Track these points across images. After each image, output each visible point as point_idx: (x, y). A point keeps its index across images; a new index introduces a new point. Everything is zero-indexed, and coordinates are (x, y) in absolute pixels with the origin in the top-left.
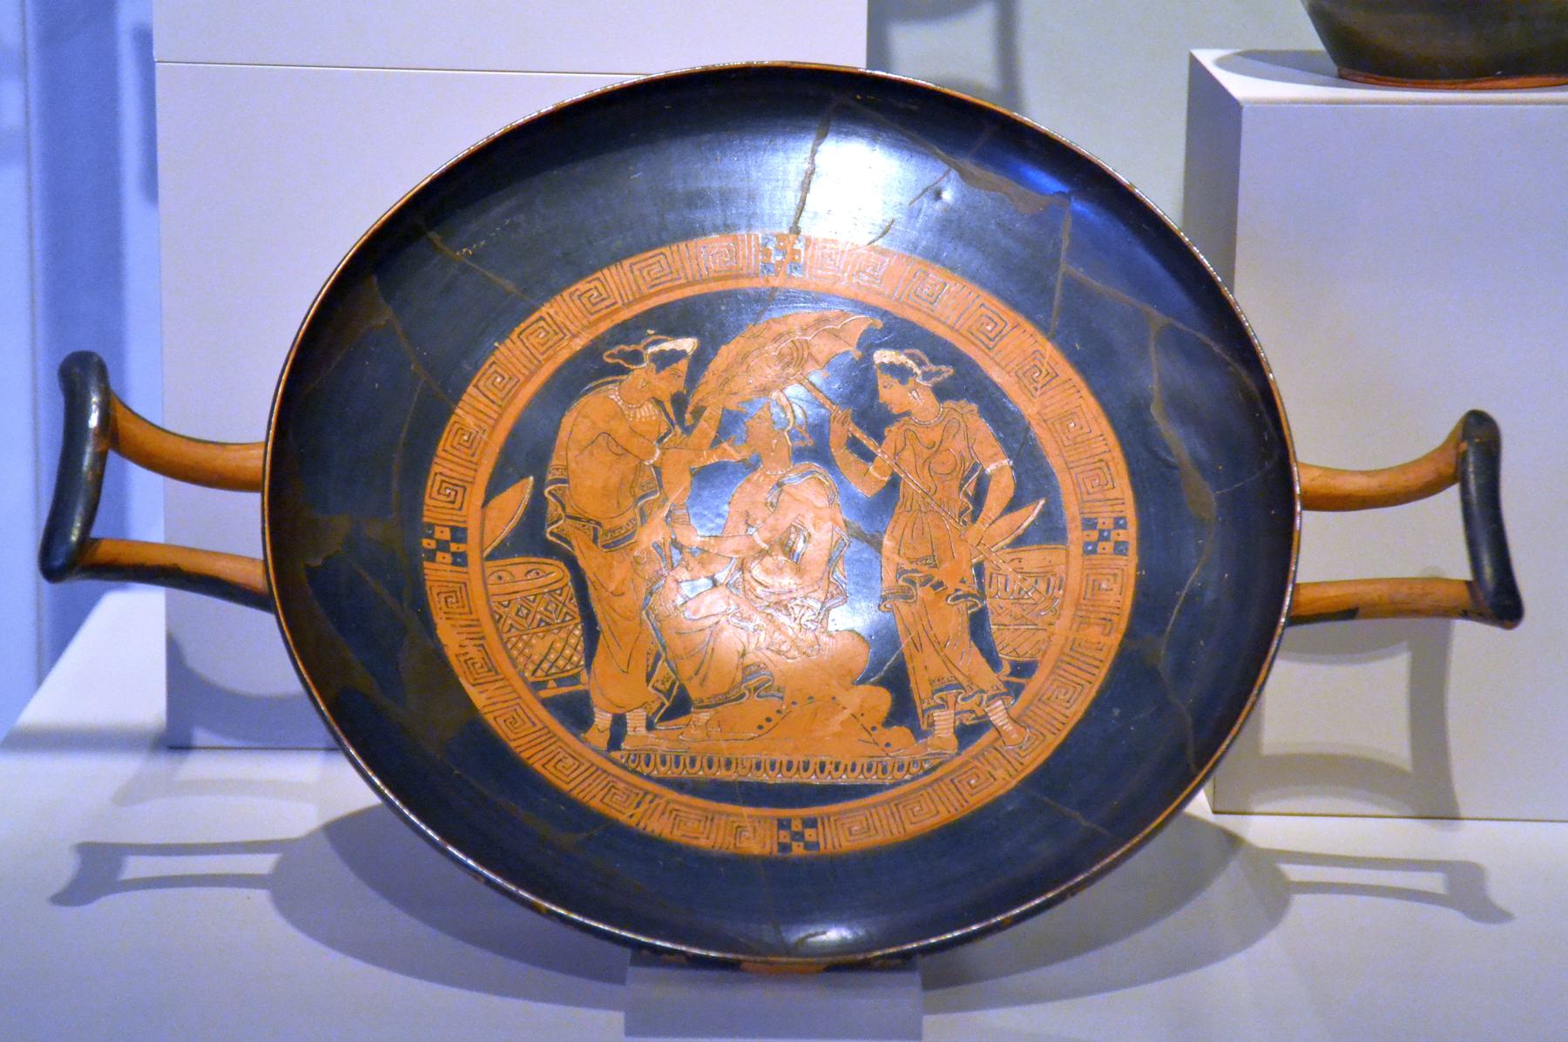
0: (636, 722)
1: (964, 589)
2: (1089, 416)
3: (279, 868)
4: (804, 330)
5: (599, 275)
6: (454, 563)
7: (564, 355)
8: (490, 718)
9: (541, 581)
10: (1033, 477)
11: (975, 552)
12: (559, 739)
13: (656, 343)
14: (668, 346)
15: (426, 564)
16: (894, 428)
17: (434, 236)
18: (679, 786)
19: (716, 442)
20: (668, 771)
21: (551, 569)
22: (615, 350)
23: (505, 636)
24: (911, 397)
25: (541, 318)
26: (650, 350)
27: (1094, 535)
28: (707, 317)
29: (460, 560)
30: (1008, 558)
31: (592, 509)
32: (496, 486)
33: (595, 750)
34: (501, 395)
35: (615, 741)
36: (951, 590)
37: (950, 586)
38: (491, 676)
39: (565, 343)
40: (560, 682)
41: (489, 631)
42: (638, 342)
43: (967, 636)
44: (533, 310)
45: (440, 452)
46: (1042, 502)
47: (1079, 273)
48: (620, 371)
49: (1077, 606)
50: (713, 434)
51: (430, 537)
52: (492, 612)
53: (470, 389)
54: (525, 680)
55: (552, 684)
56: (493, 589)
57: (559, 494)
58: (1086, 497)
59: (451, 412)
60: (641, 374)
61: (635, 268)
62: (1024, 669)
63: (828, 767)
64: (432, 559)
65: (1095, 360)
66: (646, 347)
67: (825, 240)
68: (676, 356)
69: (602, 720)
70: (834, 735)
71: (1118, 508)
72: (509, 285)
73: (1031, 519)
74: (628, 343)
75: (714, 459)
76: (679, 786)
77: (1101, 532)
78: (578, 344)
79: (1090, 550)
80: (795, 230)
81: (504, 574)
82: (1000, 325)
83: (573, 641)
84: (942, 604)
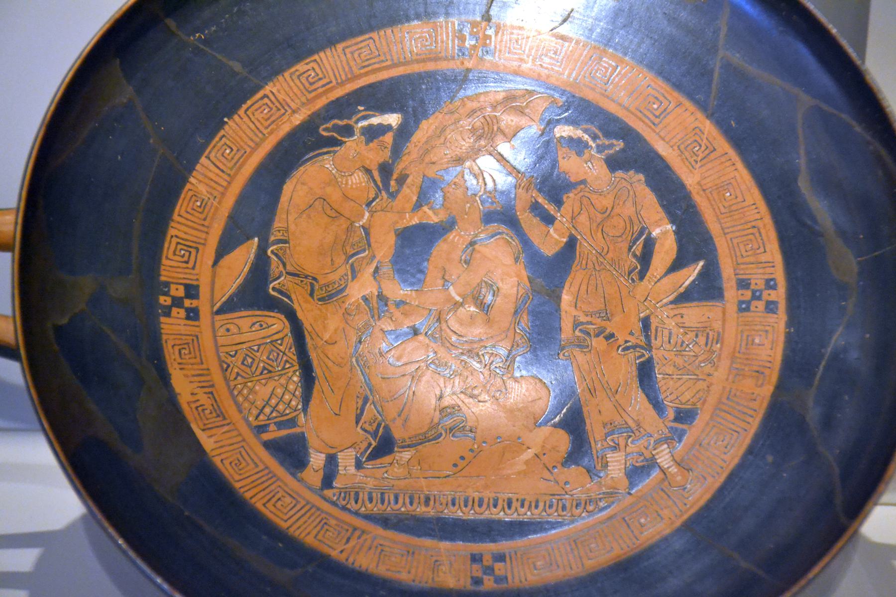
0: (346, 461)
1: (633, 341)
2: (743, 187)
3: (40, 563)
4: (494, 108)
5: (316, 57)
6: (188, 318)
7: (285, 129)
8: (217, 461)
9: (263, 333)
10: (694, 242)
11: (642, 307)
12: (279, 479)
13: (365, 118)
14: (375, 121)
15: (163, 319)
16: (571, 195)
17: (171, 23)
18: (385, 521)
19: (418, 206)
20: (375, 508)
21: (274, 321)
22: (329, 125)
23: (232, 384)
24: (589, 168)
25: (266, 96)
26: (360, 125)
27: (748, 294)
28: (409, 95)
29: (193, 314)
30: (672, 313)
31: (310, 266)
32: (225, 247)
33: (310, 488)
34: (230, 165)
35: (328, 481)
36: (621, 341)
37: (621, 338)
38: (218, 421)
39: (286, 118)
40: (280, 425)
41: (217, 379)
42: (350, 118)
43: (636, 384)
44: (259, 88)
45: (175, 217)
46: (701, 263)
47: (736, 58)
48: (333, 142)
49: (733, 358)
50: (415, 198)
51: (166, 294)
52: (221, 362)
53: (203, 160)
54: (246, 420)
55: (272, 427)
56: (221, 341)
57: (280, 253)
58: (740, 260)
59: (185, 180)
60: (353, 145)
61: (347, 51)
62: (685, 416)
63: (515, 504)
64: (168, 314)
65: (751, 138)
66: (357, 122)
67: (513, 27)
68: (383, 129)
69: (317, 460)
70: (519, 473)
71: (769, 270)
72: (237, 66)
73: (691, 279)
74: (341, 118)
75: (415, 221)
76: (385, 521)
77: (754, 292)
78: (298, 119)
79: (744, 307)
80: (487, 17)
81: (232, 327)
82: (665, 104)
83: (291, 387)
84: (614, 354)
